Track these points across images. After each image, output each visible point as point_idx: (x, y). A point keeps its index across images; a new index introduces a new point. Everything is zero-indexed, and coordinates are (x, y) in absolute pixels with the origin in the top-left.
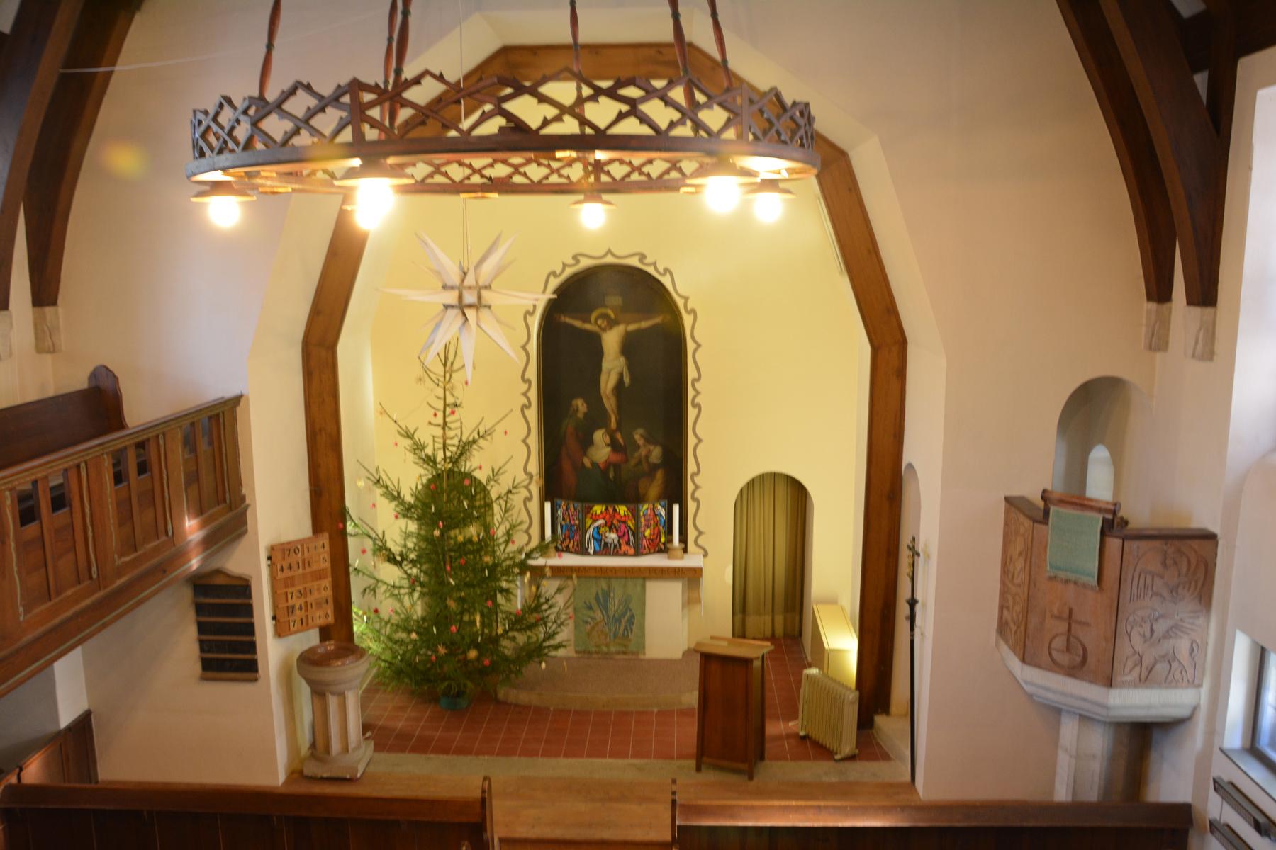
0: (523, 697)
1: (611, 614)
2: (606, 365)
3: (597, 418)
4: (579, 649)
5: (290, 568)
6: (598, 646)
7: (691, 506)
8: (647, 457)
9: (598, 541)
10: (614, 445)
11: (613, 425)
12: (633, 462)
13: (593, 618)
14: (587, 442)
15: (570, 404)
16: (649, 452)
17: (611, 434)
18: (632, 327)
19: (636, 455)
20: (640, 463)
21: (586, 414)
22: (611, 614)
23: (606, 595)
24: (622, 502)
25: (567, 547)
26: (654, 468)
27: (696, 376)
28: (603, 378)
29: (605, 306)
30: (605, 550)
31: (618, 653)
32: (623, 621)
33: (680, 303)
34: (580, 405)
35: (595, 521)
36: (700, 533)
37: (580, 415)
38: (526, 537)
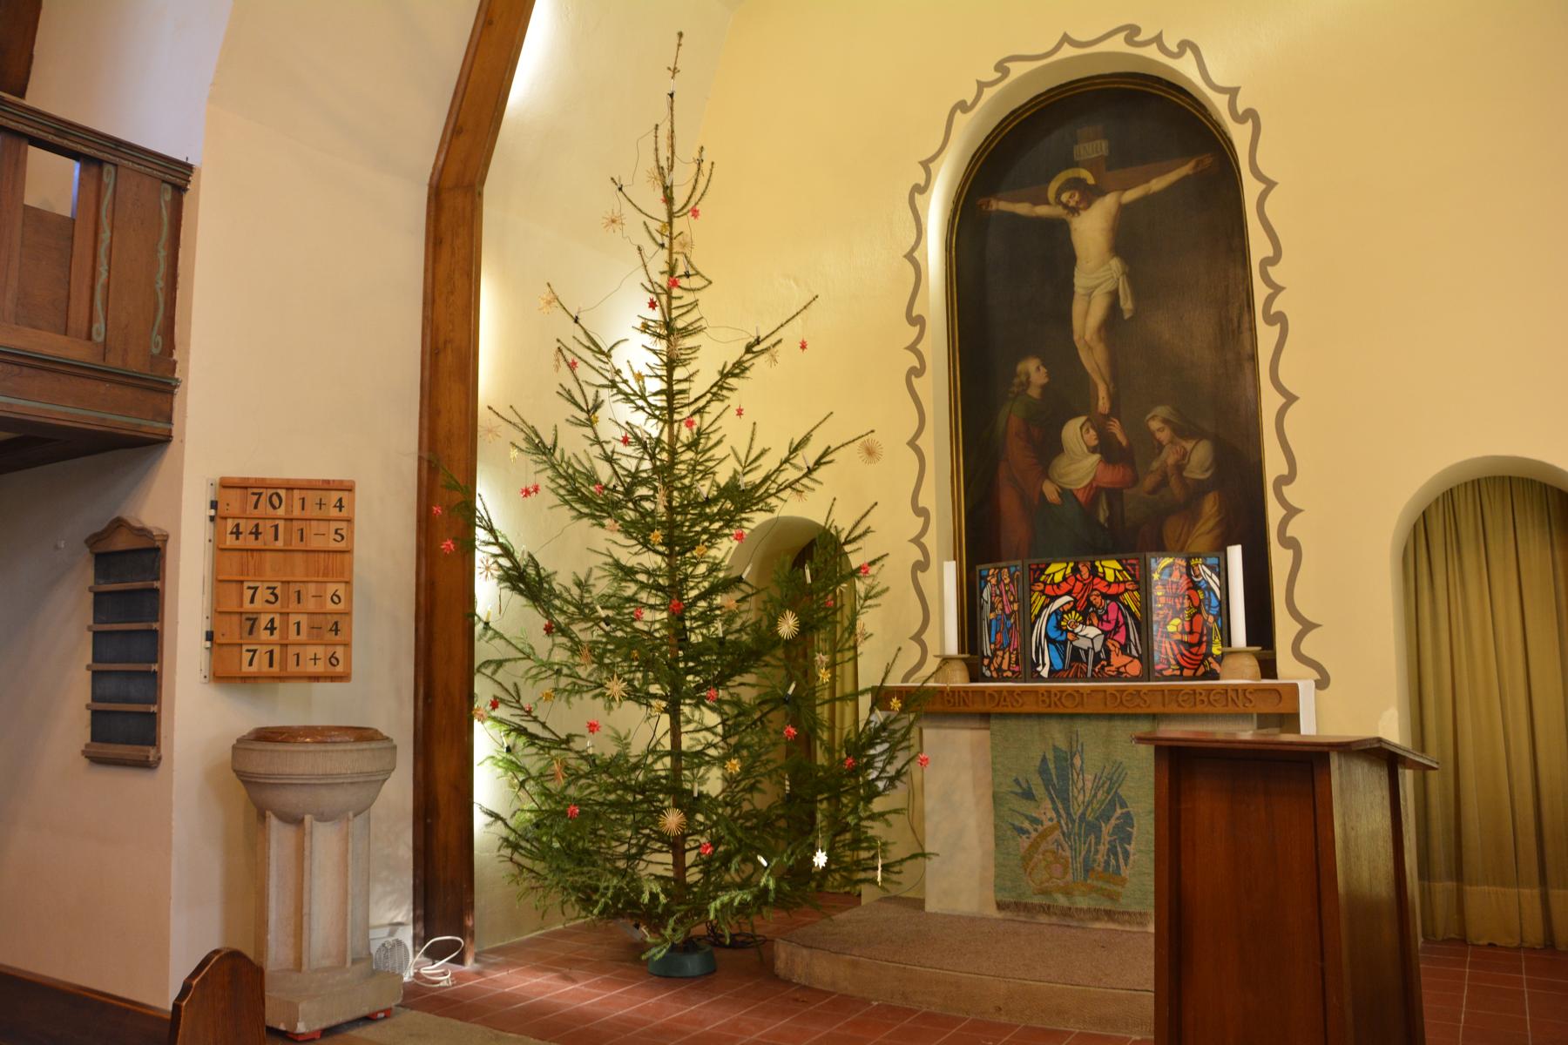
0: (822, 969)
1: (1077, 811)
2: (1081, 281)
3: (1068, 395)
4: (1008, 898)
5: (256, 533)
6: (1045, 892)
7: (1280, 559)
8: (1180, 467)
10: (1106, 448)
11: (1103, 404)
12: (1149, 482)
13: (1035, 821)
14: (1049, 448)
15: (1014, 374)
16: (1185, 455)
18: (1130, 195)
19: (1155, 465)
20: (1164, 482)
21: (1044, 388)
22: (1077, 811)
23: (1065, 761)
24: (1106, 553)
25: (999, 669)
26: (1197, 492)
27: (1269, 252)
29: (1076, 165)
31: (1097, 914)
32: (1106, 829)
33: (1219, 104)
34: (1033, 371)
35: (1054, 598)
36: (1308, 626)
37: (1034, 392)
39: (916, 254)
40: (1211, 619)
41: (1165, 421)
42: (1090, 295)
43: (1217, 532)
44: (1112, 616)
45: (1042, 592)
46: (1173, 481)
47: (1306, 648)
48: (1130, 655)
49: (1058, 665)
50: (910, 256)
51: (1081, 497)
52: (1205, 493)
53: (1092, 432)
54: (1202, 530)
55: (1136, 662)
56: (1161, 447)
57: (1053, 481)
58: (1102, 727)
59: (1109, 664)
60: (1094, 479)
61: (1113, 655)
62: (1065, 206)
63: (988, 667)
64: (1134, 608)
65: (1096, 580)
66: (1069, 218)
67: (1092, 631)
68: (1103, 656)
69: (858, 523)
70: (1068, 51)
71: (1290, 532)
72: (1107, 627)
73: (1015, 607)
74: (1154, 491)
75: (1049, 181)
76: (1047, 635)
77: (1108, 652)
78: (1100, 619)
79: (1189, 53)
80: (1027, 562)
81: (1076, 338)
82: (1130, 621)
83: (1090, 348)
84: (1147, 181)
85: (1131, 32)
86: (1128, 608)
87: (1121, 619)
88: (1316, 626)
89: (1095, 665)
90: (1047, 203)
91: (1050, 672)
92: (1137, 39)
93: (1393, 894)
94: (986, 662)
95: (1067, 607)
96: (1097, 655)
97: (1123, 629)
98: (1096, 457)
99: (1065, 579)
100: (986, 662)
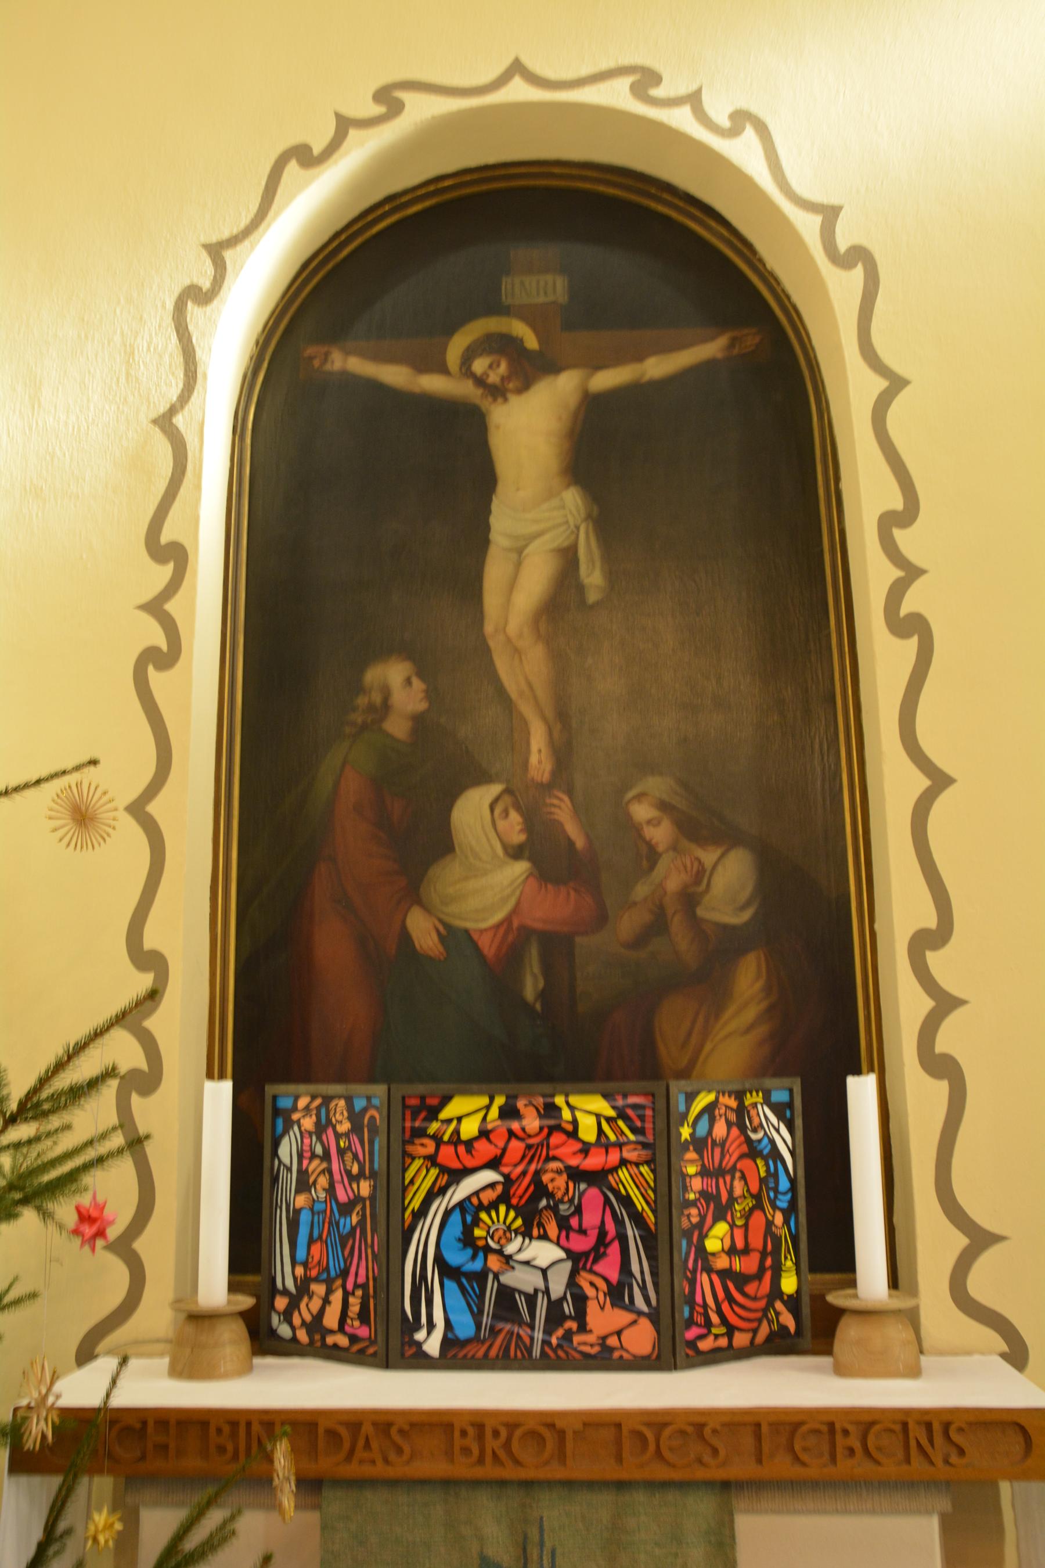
2: (504, 522)
8: (690, 899)
9: (469, 1282)
10: (545, 855)
12: (628, 924)
14: (421, 843)
15: (358, 687)
16: (701, 874)
17: (526, 799)
18: (606, 380)
19: (641, 891)
20: (658, 925)
21: (419, 721)
24: (584, 1076)
25: (315, 1326)
26: (723, 948)
28: (495, 571)
29: (505, 311)
30: (507, 1329)
35: (457, 1175)
36: (980, 1240)
37: (397, 727)
38: (119, 1274)
39: (179, 420)
40: (779, 1219)
41: (664, 806)
42: (520, 551)
43: (763, 1030)
44: (591, 1219)
45: (432, 1160)
46: (677, 924)
47: (980, 1285)
48: (631, 1307)
49: (465, 1327)
50: (165, 422)
51: (488, 946)
52: (742, 951)
53: (515, 817)
54: (732, 1026)
55: (645, 1324)
56: (653, 855)
57: (427, 910)
58: (602, 1506)
59: (583, 1328)
60: (515, 911)
61: (592, 1307)
62: (480, 381)
63: (286, 1317)
64: (640, 1203)
65: (556, 1139)
66: (485, 404)
67: (544, 1253)
68: (568, 1308)
69: (81, 1048)
70: (518, 91)
71: (942, 1045)
72: (581, 1244)
73: (365, 1188)
74: (640, 941)
75: (450, 330)
76: (439, 1259)
77: (580, 1300)
78: (563, 1224)
79: (749, 132)
80: (401, 1090)
81: (489, 628)
82: (631, 1231)
83: (517, 652)
84: (640, 358)
85: (645, 80)
86: (627, 1201)
87: (611, 1227)
88: (996, 1239)
89: (548, 1331)
90: (444, 370)
91: (447, 1343)
92: (657, 92)
93: (735, 1517)
94: (281, 1303)
95: (487, 1197)
96: (555, 1307)
97: (614, 1249)
98: (521, 867)
99: (484, 1133)
100: (281, 1303)
